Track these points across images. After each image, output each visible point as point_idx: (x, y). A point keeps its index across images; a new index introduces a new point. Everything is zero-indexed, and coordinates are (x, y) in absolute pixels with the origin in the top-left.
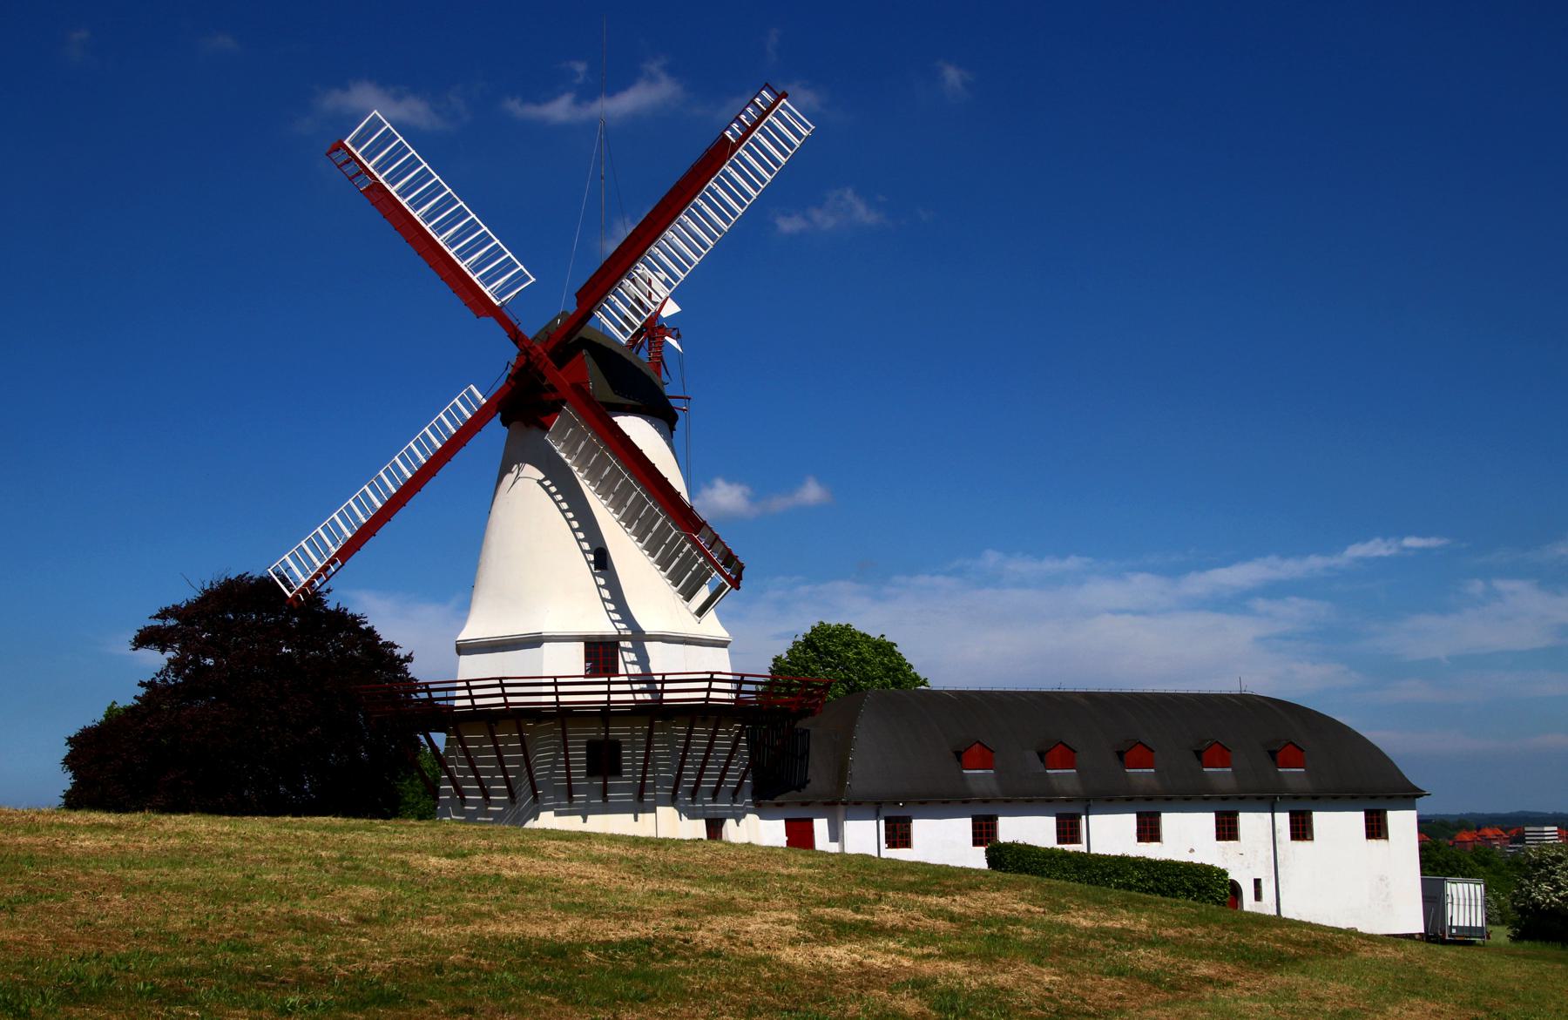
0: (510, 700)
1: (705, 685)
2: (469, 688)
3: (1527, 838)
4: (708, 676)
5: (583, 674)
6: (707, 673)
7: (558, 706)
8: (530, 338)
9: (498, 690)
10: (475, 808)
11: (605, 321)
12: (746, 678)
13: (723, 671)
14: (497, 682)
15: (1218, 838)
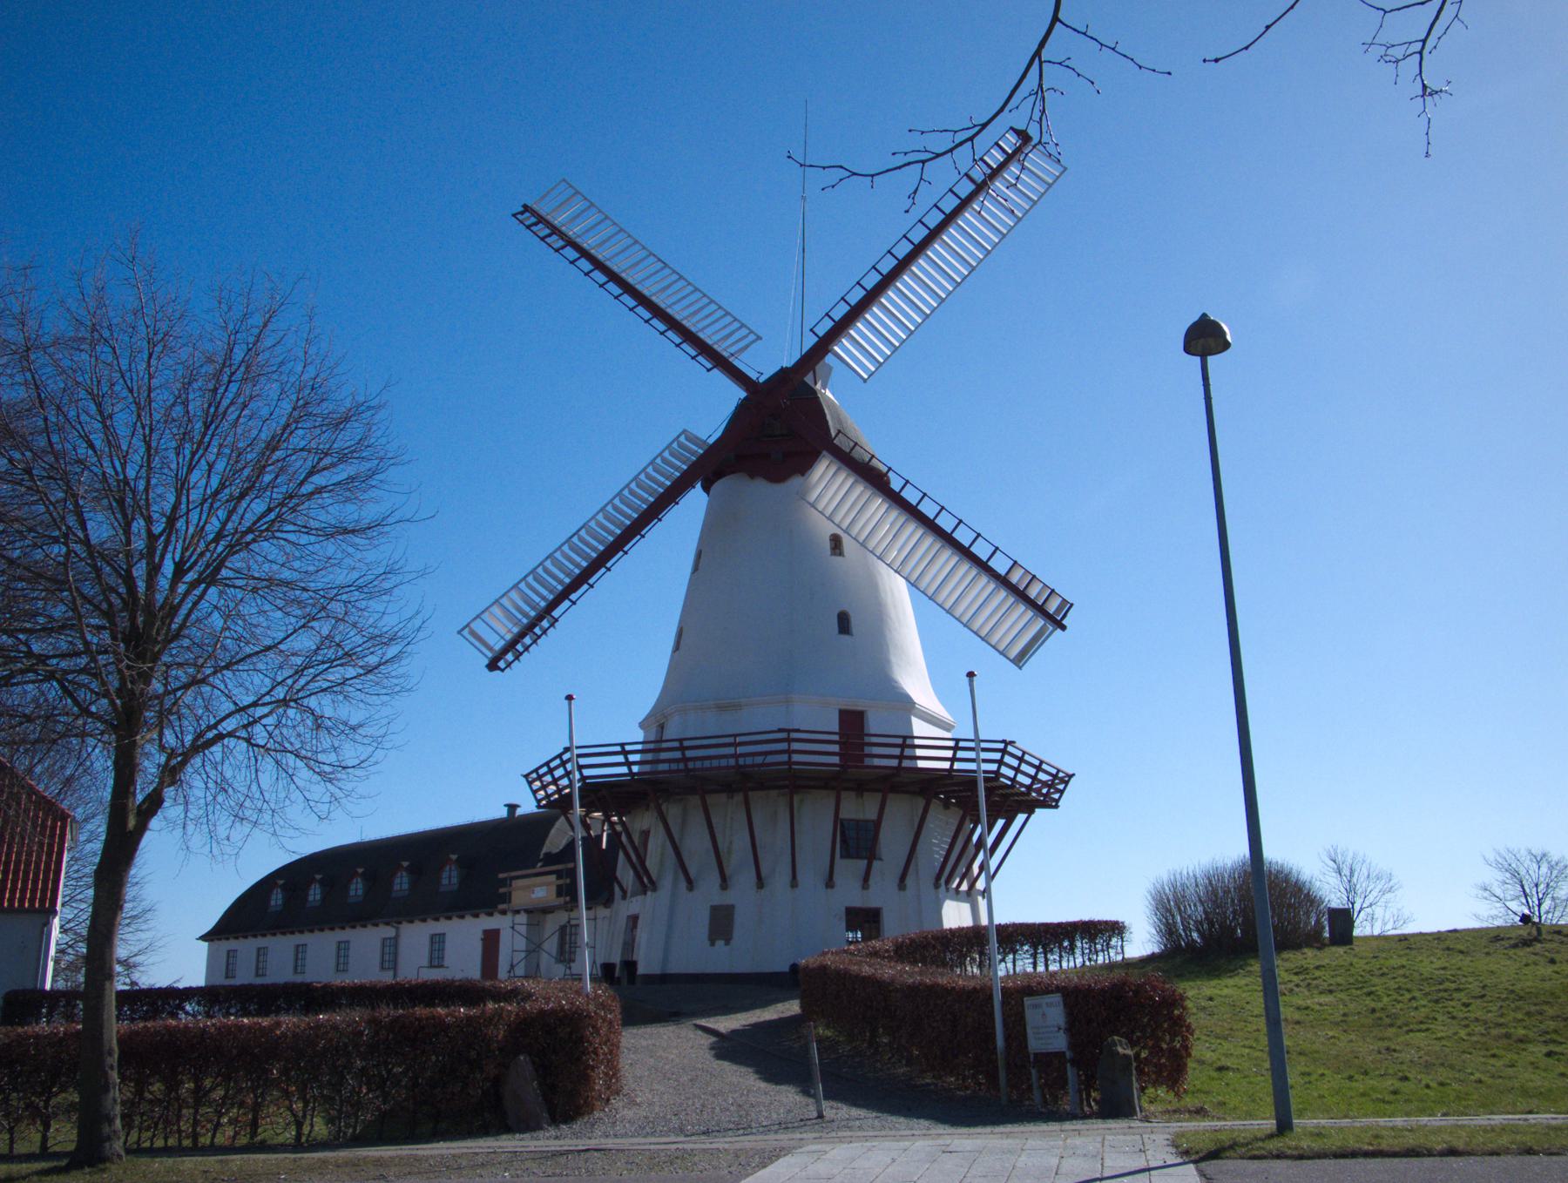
0: (796, 758)
1: (949, 754)
2: (1021, 760)
3: (836, 748)
4: (899, 741)
5: (641, 740)
6: (780, 730)
7: (633, 778)
8: (743, 394)
9: (621, 759)
10: (604, 846)
11: (877, 762)
12: (962, 744)
13: (1329, 1164)
14: (618, 749)
15: (733, 907)
